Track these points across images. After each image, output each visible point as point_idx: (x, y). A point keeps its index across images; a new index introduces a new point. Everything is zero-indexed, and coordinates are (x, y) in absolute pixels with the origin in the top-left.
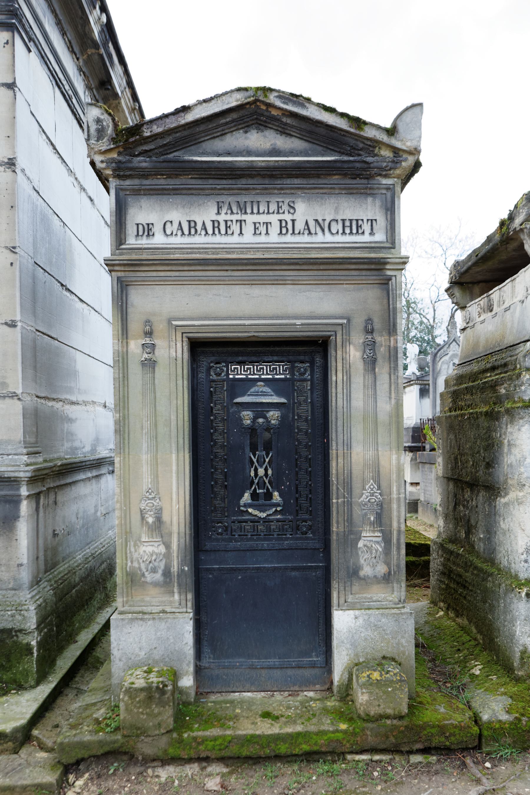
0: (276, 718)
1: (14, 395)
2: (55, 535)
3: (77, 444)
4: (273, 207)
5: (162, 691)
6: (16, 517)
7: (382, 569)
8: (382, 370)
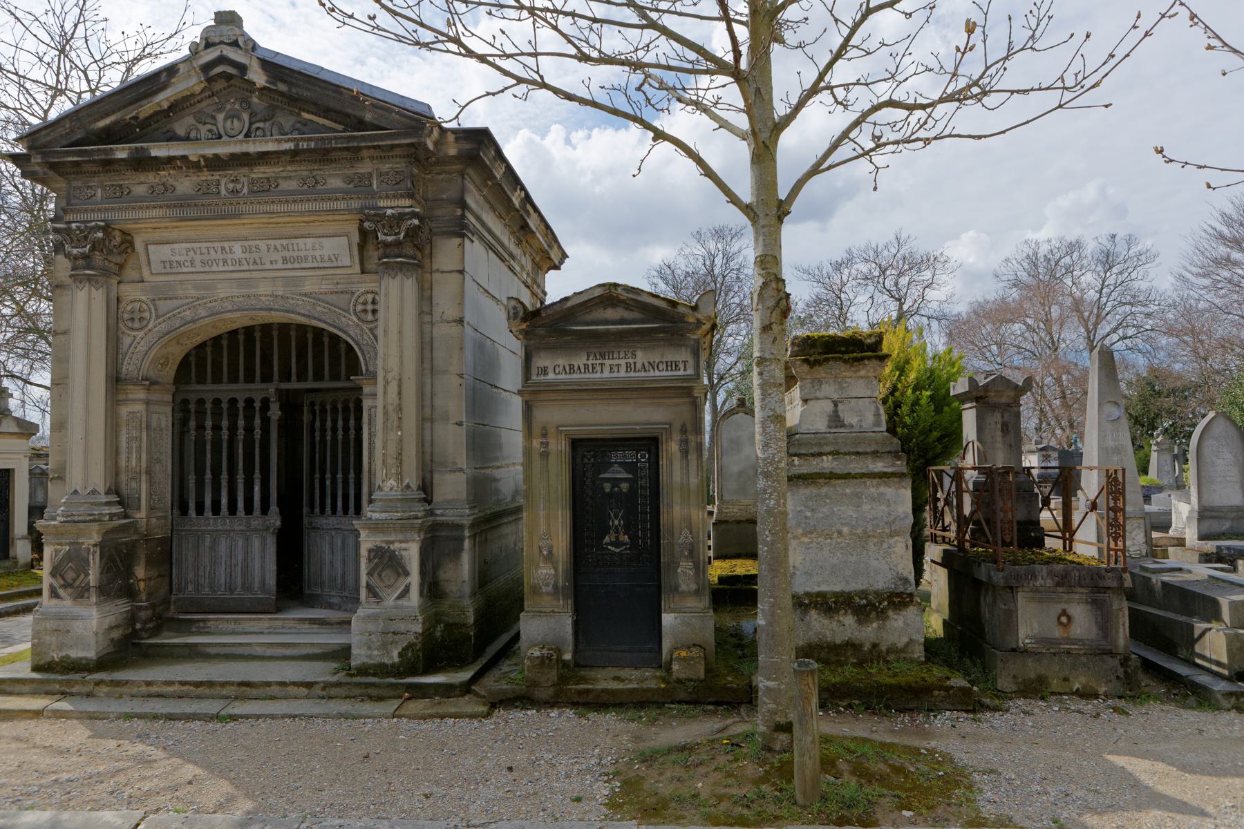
0: (623, 681)
1: (461, 470)
2: (485, 563)
3: (501, 497)
4: (622, 355)
5: (550, 659)
6: (461, 550)
7: (693, 587)
8: (693, 457)
